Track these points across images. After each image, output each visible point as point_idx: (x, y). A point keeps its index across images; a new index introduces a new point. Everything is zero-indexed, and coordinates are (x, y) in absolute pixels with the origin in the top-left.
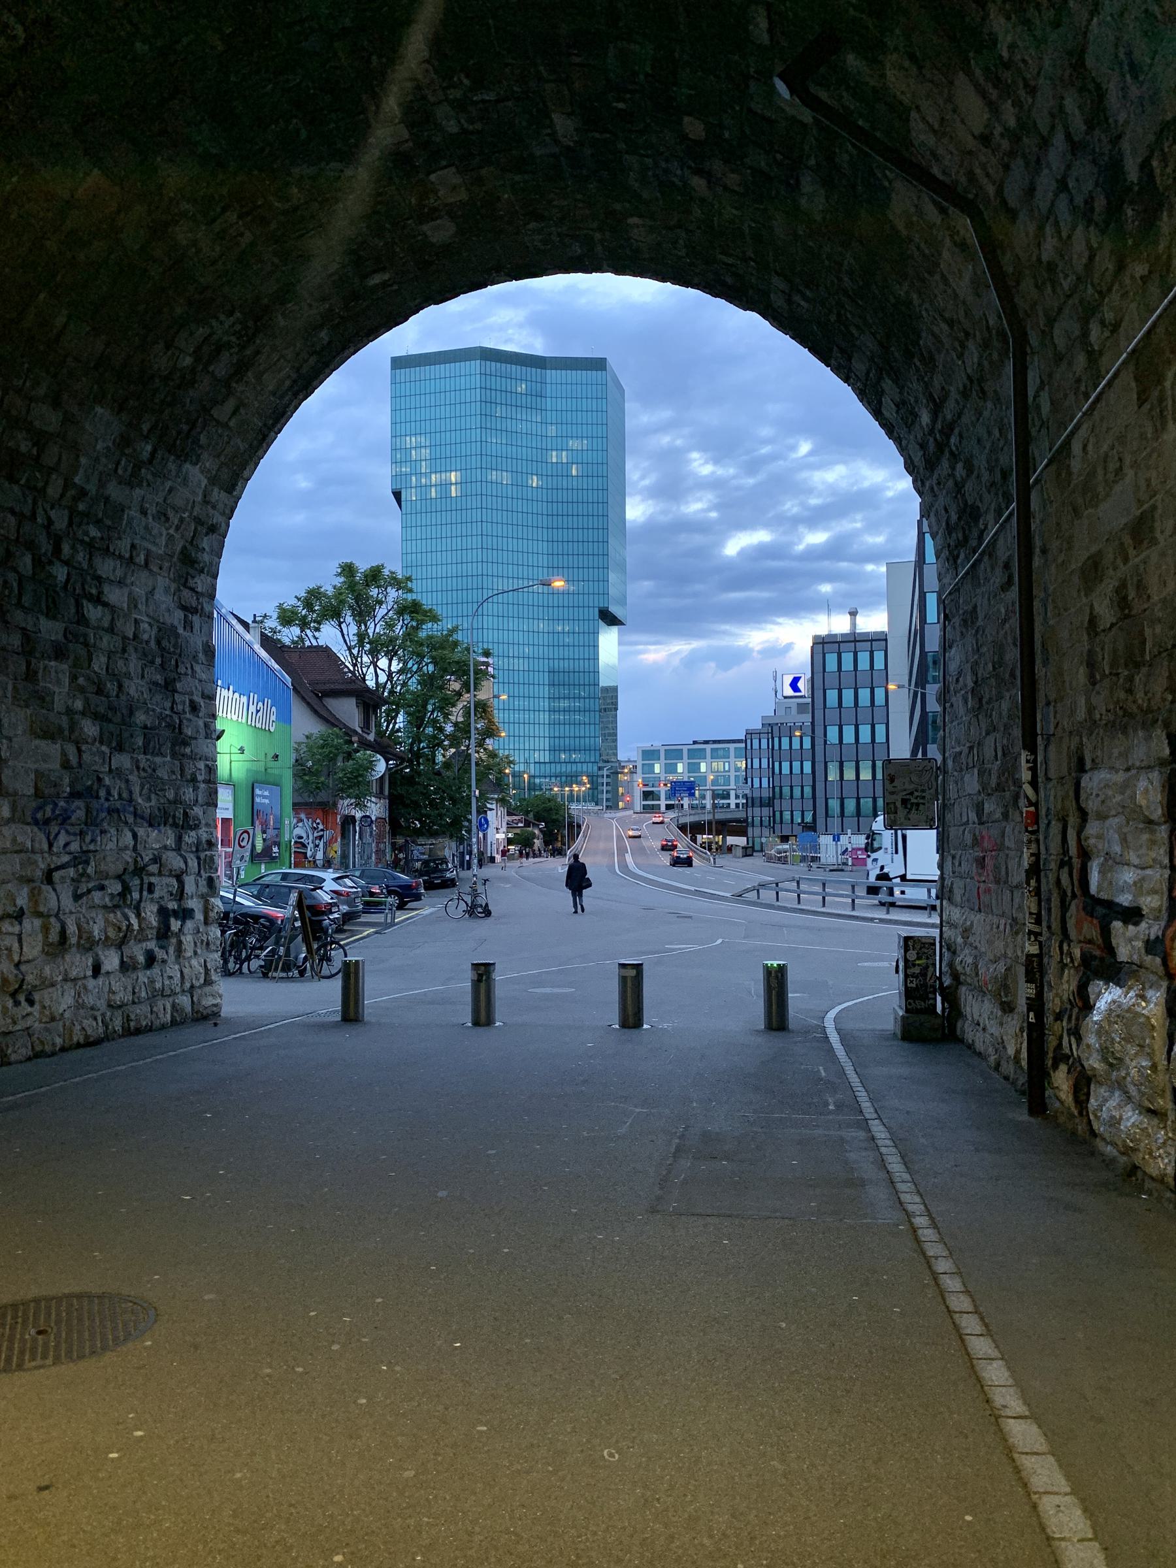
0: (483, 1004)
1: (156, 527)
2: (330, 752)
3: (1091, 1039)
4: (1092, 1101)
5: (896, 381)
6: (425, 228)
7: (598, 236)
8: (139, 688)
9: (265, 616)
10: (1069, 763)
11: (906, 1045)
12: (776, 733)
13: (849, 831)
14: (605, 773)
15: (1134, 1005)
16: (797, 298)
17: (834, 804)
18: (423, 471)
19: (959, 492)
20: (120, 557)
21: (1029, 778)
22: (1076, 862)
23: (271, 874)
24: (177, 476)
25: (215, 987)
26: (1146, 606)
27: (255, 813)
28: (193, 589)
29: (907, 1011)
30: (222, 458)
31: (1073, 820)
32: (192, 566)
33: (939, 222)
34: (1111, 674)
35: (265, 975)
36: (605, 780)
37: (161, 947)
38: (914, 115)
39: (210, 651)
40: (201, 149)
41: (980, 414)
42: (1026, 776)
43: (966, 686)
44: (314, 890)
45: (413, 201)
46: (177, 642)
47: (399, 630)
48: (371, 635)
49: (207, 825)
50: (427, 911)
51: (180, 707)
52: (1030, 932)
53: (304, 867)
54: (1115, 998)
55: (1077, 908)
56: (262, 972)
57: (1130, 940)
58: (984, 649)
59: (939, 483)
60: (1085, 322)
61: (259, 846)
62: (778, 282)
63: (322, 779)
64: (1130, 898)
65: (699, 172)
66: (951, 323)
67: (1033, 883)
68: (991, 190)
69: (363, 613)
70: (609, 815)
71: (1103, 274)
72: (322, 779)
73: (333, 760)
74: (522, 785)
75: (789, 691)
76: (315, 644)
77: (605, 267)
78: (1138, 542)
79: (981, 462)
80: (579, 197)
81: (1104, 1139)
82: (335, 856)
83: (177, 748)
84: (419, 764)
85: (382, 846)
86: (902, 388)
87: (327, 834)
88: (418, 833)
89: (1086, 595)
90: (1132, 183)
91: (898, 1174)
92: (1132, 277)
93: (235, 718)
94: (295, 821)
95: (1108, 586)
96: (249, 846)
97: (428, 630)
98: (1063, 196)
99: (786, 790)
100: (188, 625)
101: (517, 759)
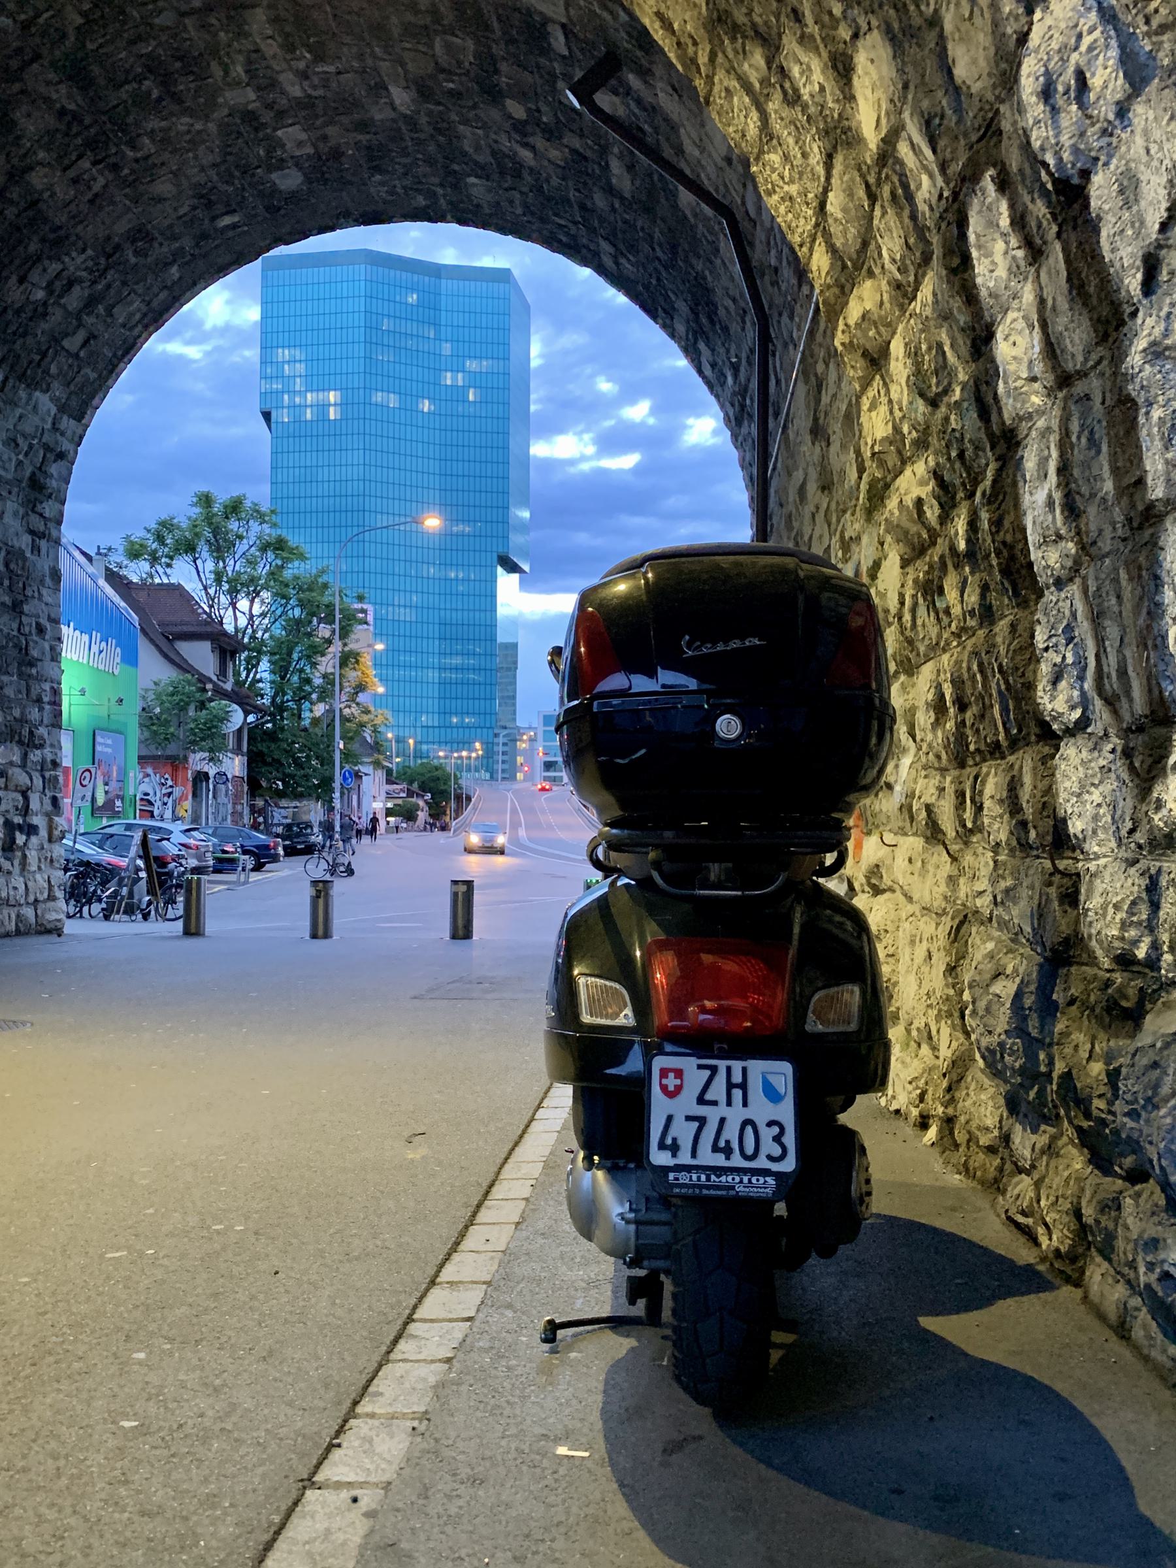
2: (181, 700)
6: (274, 176)
7: (440, 191)
9: (110, 549)
14: (501, 740)
16: (623, 261)
24: (27, 403)
28: (41, 515)
30: (72, 387)
35: (107, 918)
36: (501, 748)
37: (7, 859)
39: (56, 575)
40: (58, 106)
44: (159, 841)
45: (262, 152)
46: (24, 565)
47: (262, 570)
48: (230, 573)
49: (52, 746)
51: (27, 629)
61: (101, 800)
62: (605, 246)
63: (172, 730)
65: (526, 145)
66: (734, 300)
69: (221, 547)
73: (183, 709)
76: (166, 581)
77: (449, 217)
80: (420, 156)
82: (185, 815)
84: (282, 718)
85: (239, 807)
86: (713, 350)
87: (177, 791)
88: (281, 794)
93: (75, 658)
94: (141, 775)
96: (90, 786)
97: (294, 570)
100: (36, 549)
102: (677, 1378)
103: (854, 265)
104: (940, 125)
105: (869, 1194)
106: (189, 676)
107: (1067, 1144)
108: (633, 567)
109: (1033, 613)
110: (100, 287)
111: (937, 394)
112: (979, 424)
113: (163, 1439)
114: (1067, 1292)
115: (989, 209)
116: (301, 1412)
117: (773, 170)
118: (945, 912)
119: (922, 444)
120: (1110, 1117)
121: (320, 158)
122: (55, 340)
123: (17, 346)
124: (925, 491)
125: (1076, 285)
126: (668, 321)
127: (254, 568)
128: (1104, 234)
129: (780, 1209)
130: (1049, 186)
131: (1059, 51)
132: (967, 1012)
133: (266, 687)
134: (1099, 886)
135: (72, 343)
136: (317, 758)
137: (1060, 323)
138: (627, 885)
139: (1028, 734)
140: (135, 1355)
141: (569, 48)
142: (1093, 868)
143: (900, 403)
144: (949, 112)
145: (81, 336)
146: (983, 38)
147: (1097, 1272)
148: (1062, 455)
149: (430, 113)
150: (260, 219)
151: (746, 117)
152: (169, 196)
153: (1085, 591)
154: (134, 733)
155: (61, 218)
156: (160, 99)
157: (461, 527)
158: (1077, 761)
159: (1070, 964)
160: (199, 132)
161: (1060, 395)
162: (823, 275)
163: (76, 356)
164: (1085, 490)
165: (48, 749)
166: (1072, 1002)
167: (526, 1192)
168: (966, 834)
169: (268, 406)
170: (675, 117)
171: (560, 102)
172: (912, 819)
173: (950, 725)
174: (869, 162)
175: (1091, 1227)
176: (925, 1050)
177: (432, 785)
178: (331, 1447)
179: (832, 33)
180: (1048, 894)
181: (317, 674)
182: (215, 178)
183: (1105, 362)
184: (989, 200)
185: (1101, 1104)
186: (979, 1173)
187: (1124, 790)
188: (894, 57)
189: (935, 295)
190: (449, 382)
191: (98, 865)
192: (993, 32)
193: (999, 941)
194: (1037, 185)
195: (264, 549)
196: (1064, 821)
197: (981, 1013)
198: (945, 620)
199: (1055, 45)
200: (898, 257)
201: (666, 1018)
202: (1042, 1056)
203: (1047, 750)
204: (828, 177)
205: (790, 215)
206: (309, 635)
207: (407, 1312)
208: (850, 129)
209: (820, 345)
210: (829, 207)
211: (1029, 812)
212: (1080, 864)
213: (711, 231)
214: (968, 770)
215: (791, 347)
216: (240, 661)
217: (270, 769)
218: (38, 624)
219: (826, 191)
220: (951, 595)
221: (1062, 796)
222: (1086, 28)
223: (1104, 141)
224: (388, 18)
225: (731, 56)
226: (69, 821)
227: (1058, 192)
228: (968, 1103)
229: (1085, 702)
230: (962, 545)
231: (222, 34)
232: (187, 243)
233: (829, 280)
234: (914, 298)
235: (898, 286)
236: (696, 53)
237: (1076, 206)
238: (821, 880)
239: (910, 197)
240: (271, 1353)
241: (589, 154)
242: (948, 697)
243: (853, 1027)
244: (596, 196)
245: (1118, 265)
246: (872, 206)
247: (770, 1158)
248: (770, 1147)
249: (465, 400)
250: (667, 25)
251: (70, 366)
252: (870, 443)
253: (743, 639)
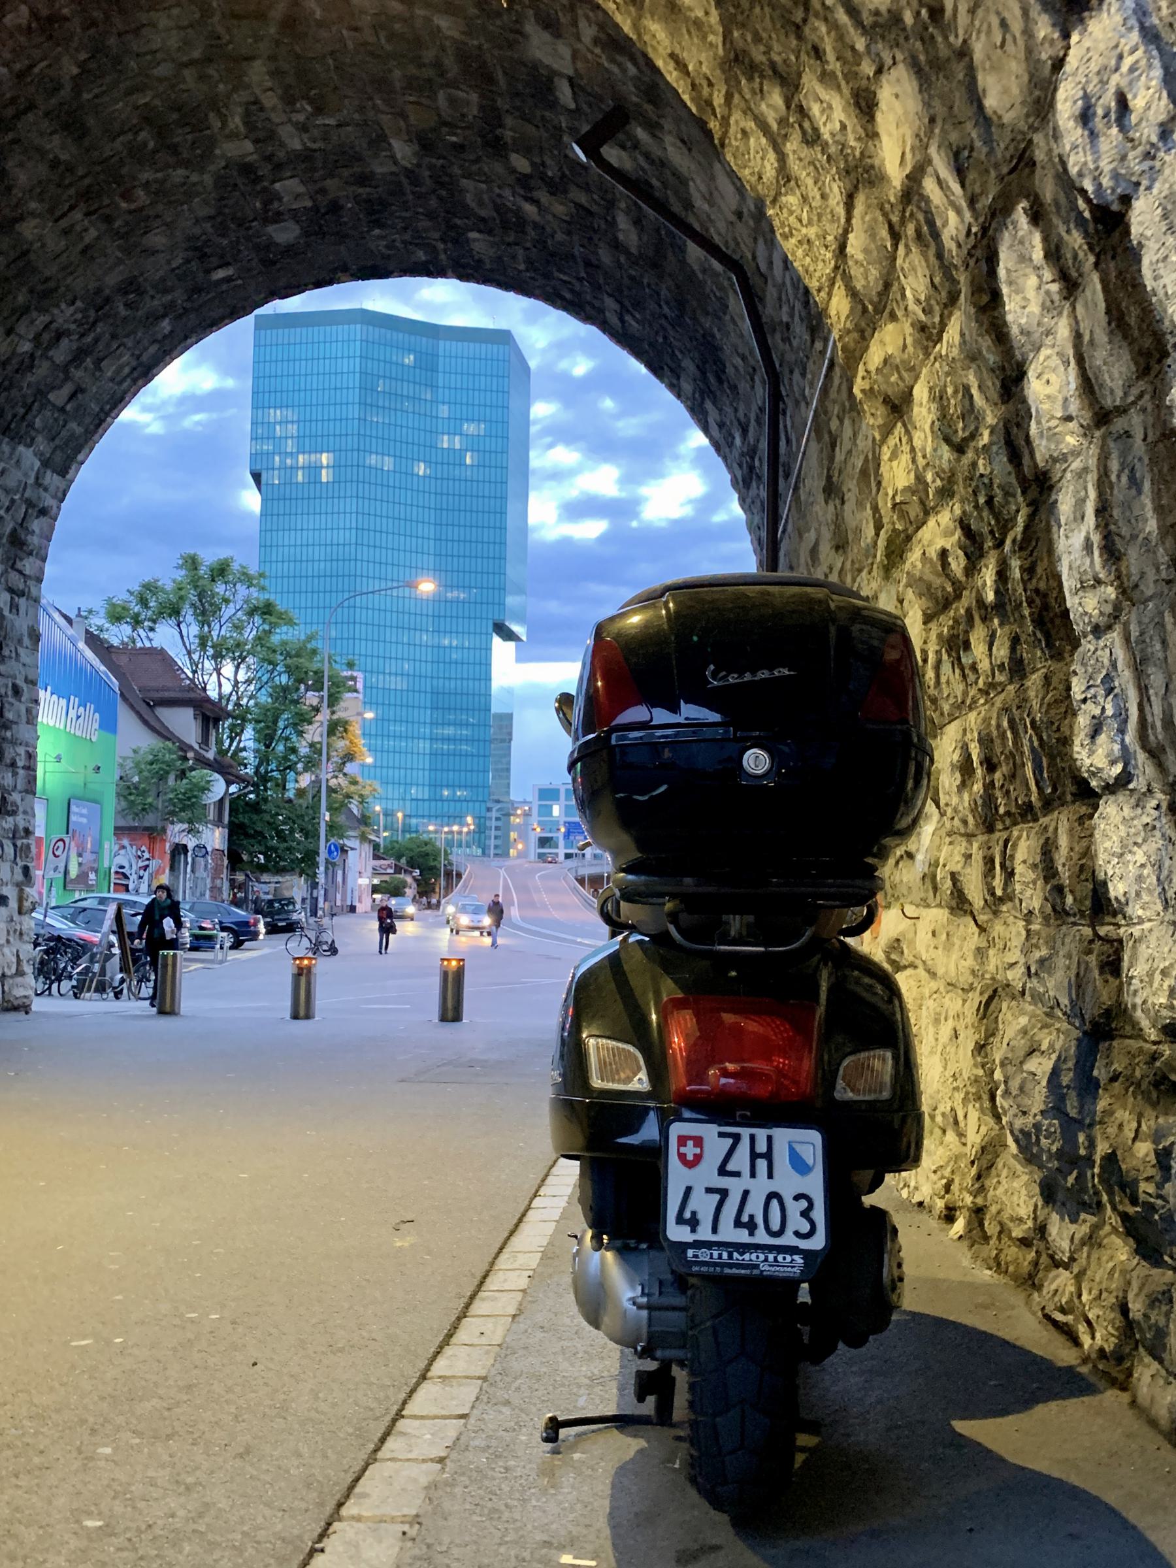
5: (714, 403)
6: (270, 229)
7: (441, 246)
9: (90, 612)
14: (494, 814)
24: (10, 458)
28: (20, 572)
30: (57, 442)
35: (76, 996)
36: (494, 823)
39: (35, 636)
47: (250, 634)
49: (25, 812)
61: (74, 872)
62: (610, 303)
63: (150, 800)
65: (527, 199)
66: (744, 358)
69: (206, 612)
70: (496, 862)
73: (163, 778)
76: (148, 645)
84: (266, 789)
85: (218, 882)
86: (720, 410)
87: (154, 864)
88: (263, 869)
93: (51, 723)
100: (14, 607)
102: (693, 1480)
103: (875, 310)
104: (969, 157)
105: (901, 1279)
106: (169, 744)
107: (1109, 1234)
108: (650, 599)
109: (1068, 665)
111: (963, 439)
112: (1010, 468)
113: (130, 1540)
114: (1112, 1398)
115: (1021, 242)
116: (280, 1514)
117: (791, 213)
118: (972, 988)
119: (946, 493)
120: (1159, 1202)
121: (318, 211)
122: (41, 393)
124: (951, 542)
125: (1116, 317)
128: (1145, 262)
129: (804, 1294)
130: (1087, 214)
131: (1098, 73)
132: (999, 1092)
133: (250, 757)
134: (1144, 951)
135: (58, 397)
136: (301, 830)
137: (1099, 357)
138: (640, 942)
139: (1064, 793)
140: (101, 1450)
141: (576, 101)
142: (1137, 934)
143: (923, 449)
144: (978, 144)
146: (1016, 67)
147: (1146, 1372)
148: (1101, 495)
149: (431, 167)
151: (762, 159)
153: (1127, 639)
154: (111, 804)
155: (51, 270)
157: (455, 594)
158: (1119, 819)
159: (1112, 1038)
161: (1097, 434)
162: (843, 319)
163: (62, 410)
164: (1125, 531)
166: (1114, 1078)
167: (523, 1283)
168: (995, 903)
170: (684, 170)
171: (566, 156)
172: (935, 889)
173: (978, 787)
174: (892, 199)
175: (1139, 1323)
176: (951, 1136)
178: (313, 1552)
179: (855, 68)
180: (1087, 963)
181: (304, 743)
182: (210, 230)
183: (1147, 397)
184: (1020, 233)
185: (1150, 1188)
186: (1011, 1269)
187: (1170, 847)
188: (920, 91)
189: (962, 335)
190: (445, 445)
191: (70, 940)
192: (1027, 59)
193: (1033, 1016)
194: (1073, 214)
195: (251, 613)
196: (1104, 884)
197: (1014, 1093)
198: (971, 677)
199: (1094, 67)
200: (923, 298)
201: (684, 1081)
202: (1081, 1138)
203: (1084, 810)
204: (849, 219)
205: (808, 259)
206: (296, 702)
207: (396, 1408)
208: (872, 167)
209: (834, 402)
210: (849, 249)
211: (1065, 875)
212: (1122, 930)
213: (722, 288)
214: (997, 834)
215: (803, 404)
217: (252, 841)
219: (846, 232)
220: (979, 649)
221: (1101, 858)
222: (1127, 48)
223: (1146, 165)
225: (748, 96)
226: (40, 894)
227: (1096, 219)
228: (1000, 1190)
229: (1126, 756)
230: (990, 597)
232: (179, 296)
233: (848, 325)
234: (940, 339)
235: (923, 328)
236: (711, 95)
237: (1117, 234)
238: (850, 941)
239: (936, 235)
240: (248, 1450)
241: (594, 208)
242: (975, 758)
243: (886, 1095)
244: (600, 251)
245: (1161, 293)
246: (895, 246)
247: (797, 1234)
248: (798, 1223)
249: (462, 464)
250: (681, 65)
251: (56, 420)
252: (891, 493)
253: (771, 669)
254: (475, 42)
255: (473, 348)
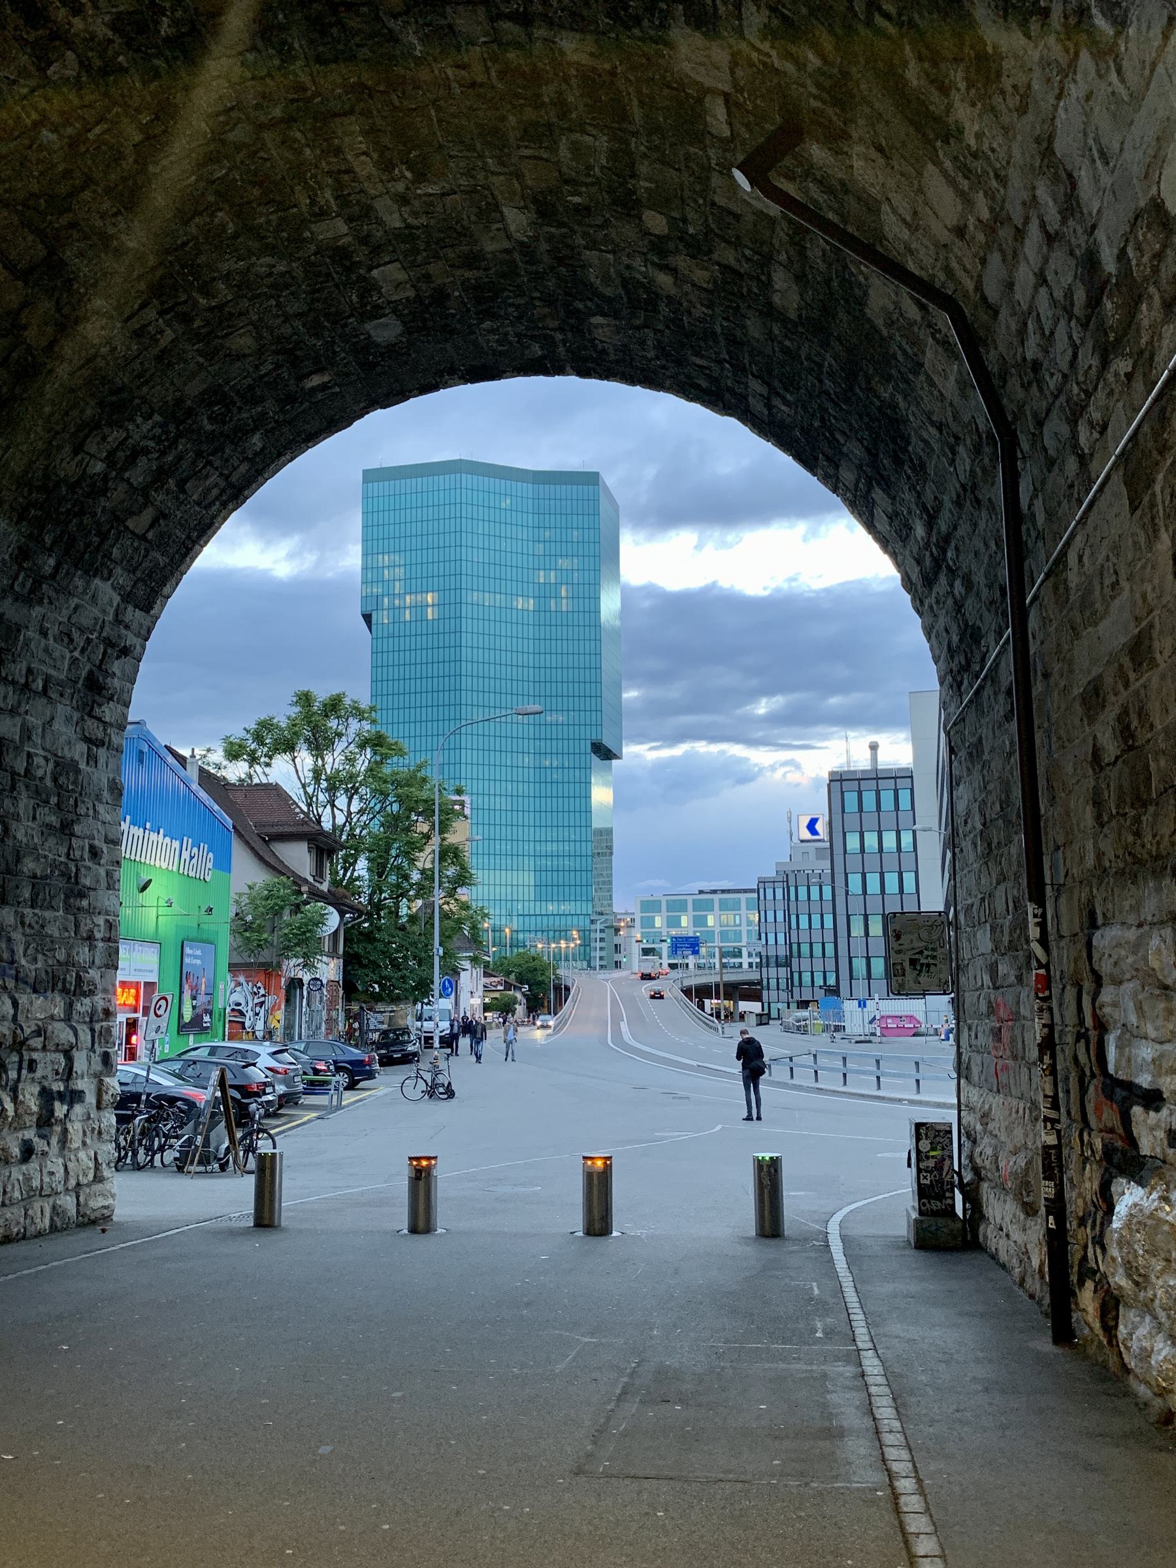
0: (421, 1208)
1: (58, 649)
3: (1114, 1251)
4: (1121, 1327)
5: (886, 491)
6: (368, 326)
7: (559, 336)
8: (29, 831)
10: (1081, 917)
11: (921, 1255)
12: (792, 882)
13: (876, 996)
14: (598, 926)
15: (1156, 1210)
16: (776, 402)
17: (859, 965)
18: (397, 591)
19: (959, 611)
20: (14, 683)
21: (1038, 936)
22: (1093, 1034)
23: (199, 1046)
24: (84, 592)
25: (108, 1186)
26: (1149, 736)
27: (183, 976)
28: (99, 719)
29: (921, 1213)
30: (139, 574)
31: (1088, 985)
32: (99, 694)
33: (918, 318)
34: (1118, 813)
35: (180, 1169)
36: (598, 954)
38: (885, 208)
41: (975, 525)
42: (1034, 932)
43: (974, 828)
44: (244, 1067)
46: (76, 779)
47: (362, 764)
48: (329, 771)
49: (105, 991)
50: (381, 1091)
51: (78, 854)
52: (1046, 1119)
53: (241, 1039)
54: (1137, 1200)
55: (1096, 1089)
56: (178, 1166)
57: (1152, 1129)
58: (990, 787)
59: (938, 602)
60: (1073, 422)
61: (188, 1016)
62: (756, 386)
63: (265, 936)
64: (1149, 1079)
66: (940, 427)
67: (1047, 1059)
68: (970, 285)
69: (320, 744)
71: (1086, 372)
72: (265, 936)
73: (277, 912)
74: (503, 941)
75: (806, 835)
76: (264, 781)
77: (568, 368)
78: (1137, 665)
79: (979, 578)
81: (1136, 1376)
82: (278, 1025)
83: (72, 900)
84: (379, 918)
85: (334, 1013)
86: (894, 499)
87: (270, 1000)
88: (377, 998)
89: (1089, 725)
90: (1110, 274)
91: (886, 1422)
92: (1116, 374)
93: (164, 866)
94: (233, 985)
95: (1110, 714)
98: (1043, 291)
99: (805, 949)
100: (92, 759)
101: (492, 912)
106: (284, 878)
110: (170, 458)
122: (118, 518)
123: (72, 527)
126: (831, 471)
127: (353, 765)
133: (364, 886)
135: (139, 523)
141: (730, 124)
145: (148, 515)
149: (550, 238)
150: (353, 378)
152: (247, 351)
154: (225, 941)
156: (236, 236)
160: (282, 274)
163: (143, 538)
165: (100, 995)
169: (369, 608)
177: (530, 975)
216: (338, 859)
217: (366, 971)
218: (92, 847)
224: (503, 119)
231: (308, 151)
251: (136, 549)
254: (607, 66)
255: (562, 490)
